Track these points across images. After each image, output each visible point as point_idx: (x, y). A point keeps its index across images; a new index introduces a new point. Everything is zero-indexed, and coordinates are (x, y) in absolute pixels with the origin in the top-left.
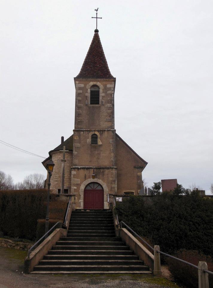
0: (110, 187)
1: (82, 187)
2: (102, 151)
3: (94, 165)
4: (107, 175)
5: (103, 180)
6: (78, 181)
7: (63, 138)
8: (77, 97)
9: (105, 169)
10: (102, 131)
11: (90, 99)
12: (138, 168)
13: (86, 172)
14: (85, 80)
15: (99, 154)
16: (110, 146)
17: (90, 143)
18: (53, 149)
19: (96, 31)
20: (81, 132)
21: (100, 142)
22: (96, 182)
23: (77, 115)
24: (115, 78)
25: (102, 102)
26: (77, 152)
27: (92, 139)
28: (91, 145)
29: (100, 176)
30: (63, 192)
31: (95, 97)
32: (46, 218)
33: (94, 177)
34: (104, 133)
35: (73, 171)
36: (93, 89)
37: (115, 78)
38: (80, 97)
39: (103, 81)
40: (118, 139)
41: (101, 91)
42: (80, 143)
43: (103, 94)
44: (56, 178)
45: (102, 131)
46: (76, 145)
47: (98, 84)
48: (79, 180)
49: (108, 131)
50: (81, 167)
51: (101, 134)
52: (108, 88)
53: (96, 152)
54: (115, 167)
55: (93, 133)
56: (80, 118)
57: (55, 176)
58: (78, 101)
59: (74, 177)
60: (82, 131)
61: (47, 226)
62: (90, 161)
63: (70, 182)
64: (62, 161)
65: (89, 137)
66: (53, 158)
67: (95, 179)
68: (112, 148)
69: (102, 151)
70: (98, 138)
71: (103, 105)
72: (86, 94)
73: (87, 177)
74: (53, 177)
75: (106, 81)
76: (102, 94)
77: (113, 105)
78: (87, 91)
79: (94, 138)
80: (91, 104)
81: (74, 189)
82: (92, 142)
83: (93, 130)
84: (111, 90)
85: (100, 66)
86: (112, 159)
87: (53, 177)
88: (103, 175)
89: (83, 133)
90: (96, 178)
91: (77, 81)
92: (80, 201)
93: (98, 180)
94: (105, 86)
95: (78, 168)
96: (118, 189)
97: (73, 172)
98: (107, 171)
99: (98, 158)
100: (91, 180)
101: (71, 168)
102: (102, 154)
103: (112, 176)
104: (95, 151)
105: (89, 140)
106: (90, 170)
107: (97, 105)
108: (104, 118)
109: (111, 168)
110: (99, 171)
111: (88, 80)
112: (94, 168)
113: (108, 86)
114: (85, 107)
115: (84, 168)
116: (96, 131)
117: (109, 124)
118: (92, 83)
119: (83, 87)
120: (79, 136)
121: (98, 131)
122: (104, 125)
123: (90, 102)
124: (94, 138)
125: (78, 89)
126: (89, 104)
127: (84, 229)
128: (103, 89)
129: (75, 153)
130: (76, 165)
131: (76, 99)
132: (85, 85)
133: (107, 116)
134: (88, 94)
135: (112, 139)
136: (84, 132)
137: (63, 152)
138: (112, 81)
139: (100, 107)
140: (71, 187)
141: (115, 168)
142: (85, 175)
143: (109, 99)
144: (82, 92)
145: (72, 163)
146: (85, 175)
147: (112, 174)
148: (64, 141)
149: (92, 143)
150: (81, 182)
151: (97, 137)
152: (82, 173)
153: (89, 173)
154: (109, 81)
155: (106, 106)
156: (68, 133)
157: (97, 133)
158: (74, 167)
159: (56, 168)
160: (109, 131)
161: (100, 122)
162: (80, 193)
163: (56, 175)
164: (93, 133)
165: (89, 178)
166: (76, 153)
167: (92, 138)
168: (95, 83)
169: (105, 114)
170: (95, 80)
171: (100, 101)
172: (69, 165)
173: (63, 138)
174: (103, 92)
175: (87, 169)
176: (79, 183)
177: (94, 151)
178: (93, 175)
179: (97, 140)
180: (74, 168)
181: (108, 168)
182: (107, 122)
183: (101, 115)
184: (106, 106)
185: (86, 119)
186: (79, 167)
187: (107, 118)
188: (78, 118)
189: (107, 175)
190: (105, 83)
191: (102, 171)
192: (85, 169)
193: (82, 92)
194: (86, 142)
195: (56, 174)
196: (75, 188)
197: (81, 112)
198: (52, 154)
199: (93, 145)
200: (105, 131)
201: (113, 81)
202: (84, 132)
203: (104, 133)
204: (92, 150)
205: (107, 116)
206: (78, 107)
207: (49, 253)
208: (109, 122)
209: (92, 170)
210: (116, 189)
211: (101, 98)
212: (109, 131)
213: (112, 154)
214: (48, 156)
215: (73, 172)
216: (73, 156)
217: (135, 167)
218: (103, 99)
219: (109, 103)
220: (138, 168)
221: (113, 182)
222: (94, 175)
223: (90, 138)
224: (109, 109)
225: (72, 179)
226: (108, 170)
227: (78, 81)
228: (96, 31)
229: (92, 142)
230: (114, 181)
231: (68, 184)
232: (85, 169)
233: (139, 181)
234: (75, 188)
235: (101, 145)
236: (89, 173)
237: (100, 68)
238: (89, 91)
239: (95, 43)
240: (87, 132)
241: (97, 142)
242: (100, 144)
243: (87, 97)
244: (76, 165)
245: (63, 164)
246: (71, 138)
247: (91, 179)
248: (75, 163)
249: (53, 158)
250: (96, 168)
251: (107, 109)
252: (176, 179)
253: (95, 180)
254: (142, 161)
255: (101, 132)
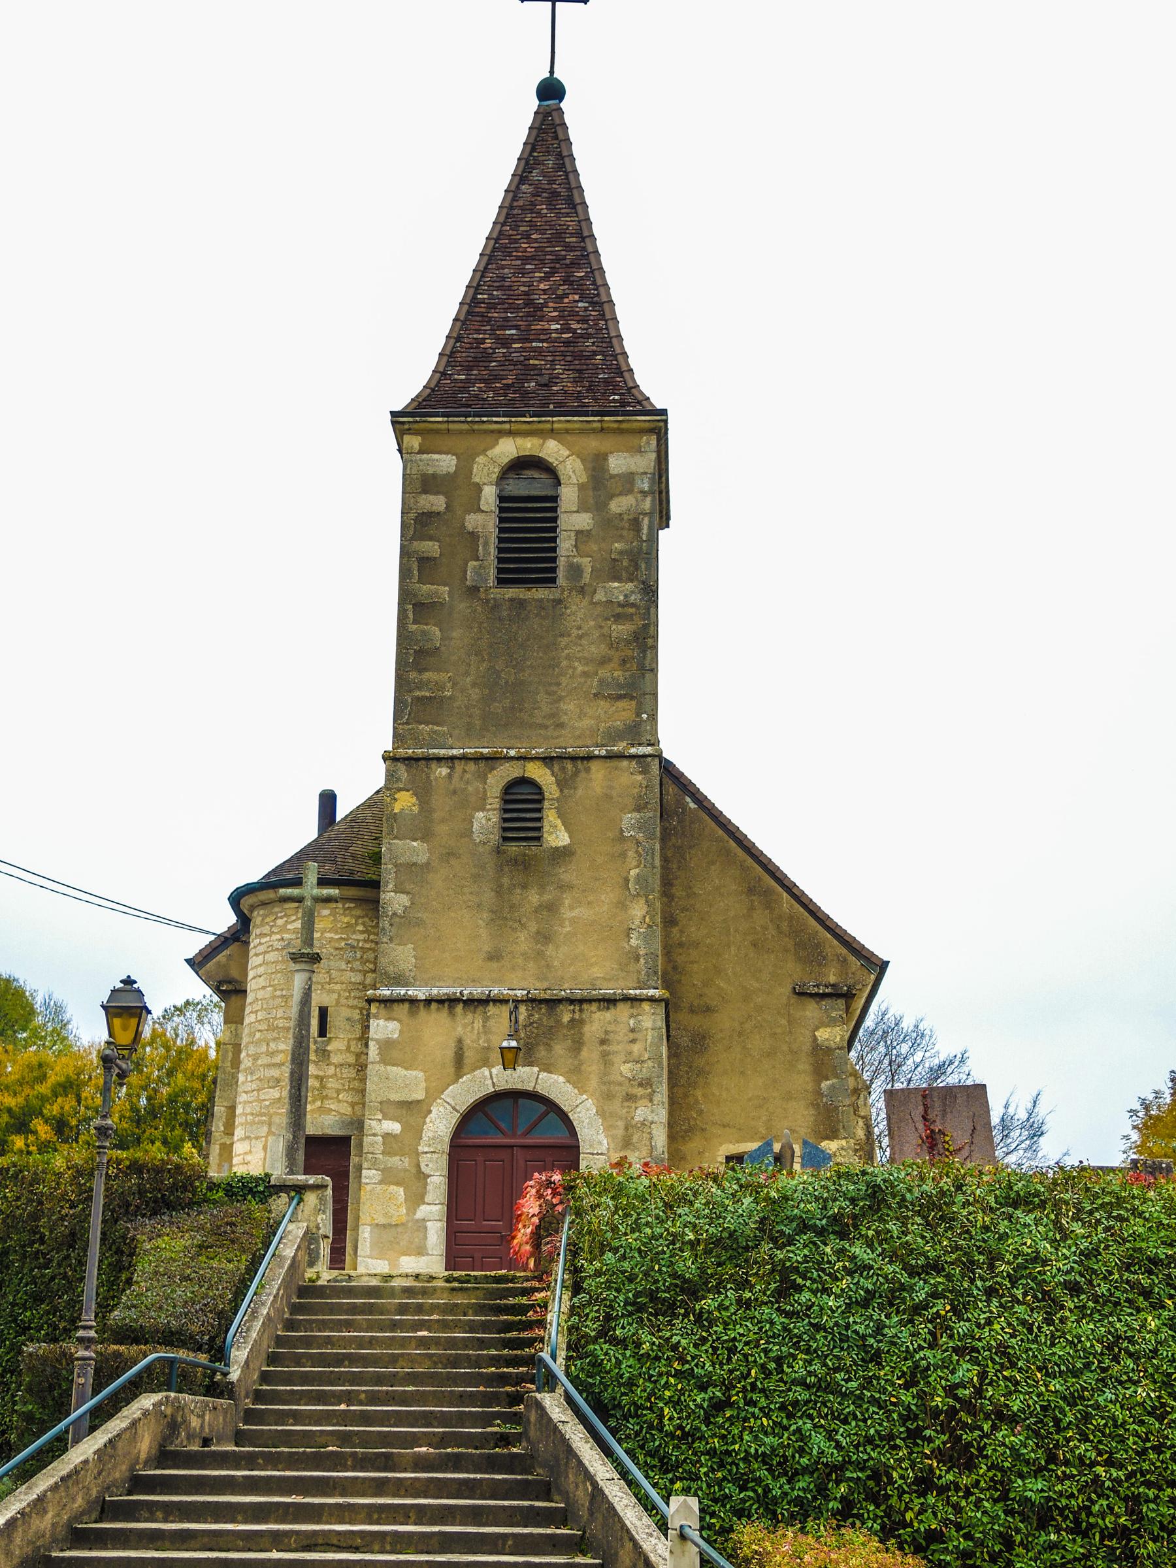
0: (621, 1124)
1: (440, 1124)
2: (571, 887)
3: (517, 983)
4: (603, 1042)
5: (575, 1075)
6: (408, 1082)
7: (328, 801)
8: (412, 539)
9: (585, 1006)
10: (569, 763)
11: (493, 551)
12: (824, 996)
13: (467, 1026)
14: (465, 427)
15: (551, 908)
16: (623, 855)
17: (495, 837)
18: (255, 876)
19: (551, 91)
20: (434, 765)
21: (557, 836)
22: (529, 1087)
23: (413, 657)
24: (664, 412)
25: (575, 571)
26: (408, 893)
27: (506, 811)
28: (498, 851)
29: (559, 1049)
30: (300, 1156)
31: (528, 538)
32: (80, 1333)
33: (510, 1059)
34: (588, 770)
35: (376, 1017)
36: (516, 488)
37: (664, 412)
38: (431, 538)
39: (582, 432)
40: (692, 805)
41: (568, 495)
42: (426, 835)
43: (584, 521)
44: (274, 1065)
45: (574, 758)
46: (405, 849)
47: (552, 450)
48: (421, 1075)
49: (610, 757)
50: (435, 991)
51: (561, 784)
52: (612, 477)
53: (534, 898)
54: (651, 992)
55: (511, 771)
56: (427, 675)
57: (264, 1049)
58: (415, 567)
59: (385, 1061)
60: (439, 759)
61: (83, 1379)
62: (494, 956)
63: (363, 1092)
64: (295, 957)
65: (484, 799)
66: (255, 931)
67: (522, 1071)
68: (633, 872)
69: (571, 887)
70: (546, 804)
71: (582, 591)
72: (473, 521)
73: (470, 1056)
74: (256, 1058)
75: (602, 429)
76: (573, 518)
77: (650, 592)
78: (479, 499)
79: (522, 806)
80: (501, 582)
81: (386, 1136)
82: (505, 829)
83: (512, 753)
84: (630, 491)
85: (566, 329)
86: (633, 942)
87: (256, 1058)
88: (578, 1045)
89: (450, 776)
90: (531, 1064)
91: (409, 431)
92: (423, 1211)
93: (543, 1075)
94: (597, 466)
95: (413, 1001)
96: (672, 1137)
97: (382, 1022)
98: (597, 1021)
99: (544, 937)
100: (492, 1078)
101: (370, 1001)
102: (571, 908)
103: (636, 1048)
104: (524, 887)
105: (485, 821)
106: (492, 1009)
107: (541, 593)
108: (584, 674)
109: (626, 999)
110: (548, 1018)
111: (485, 427)
112: (517, 1002)
113: (618, 463)
114: (462, 606)
115: (450, 1002)
116: (532, 759)
117: (623, 712)
118: (507, 449)
119: (448, 474)
120: (423, 793)
121: (547, 760)
122: (584, 720)
123: (493, 573)
124: (522, 806)
125: (416, 484)
126: (491, 581)
127: (461, 1395)
128: (582, 487)
129: (394, 900)
130: (399, 980)
131: (405, 552)
132: (466, 461)
133: (604, 661)
134: (484, 521)
135: (638, 809)
136: (452, 768)
137: (300, 900)
138: (642, 432)
139: (560, 601)
140: (367, 1122)
141: (651, 1000)
142: (460, 1041)
143: (621, 553)
144: (442, 508)
145: (375, 970)
146: (460, 1041)
147: (631, 1036)
148: (338, 818)
149: (505, 839)
150: (434, 1094)
151: (540, 801)
152: (438, 1032)
153: (486, 1030)
154: (621, 431)
155: (600, 596)
156: (663, 534)
157: (535, 771)
158: (385, 992)
159: (274, 997)
160: (621, 756)
161: (561, 699)
162: (424, 1160)
163: (273, 1046)
164: (516, 775)
165: (486, 1062)
166: (404, 899)
167: (506, 802)
168: (528, 446)
169: (593, 649)
170: (525, 427)
171: (561, 562)
172: (357, 978)
173: (328, 801)
174: (583, 508)
175: (472, 1003)
176: (419, 1095)
177: (518, 891)
178: (505, 1044)
179: (539, 819)
180: (387, 1002)
181: (609, 1002)
182: (602, 703)
183: (568, 657)
184: (600, 596)
185: (468, 680)
186: (420, 993)
187: (604, 673)
188: (413, 675)
189: (603, 1042)
190: (594, 444)
191: (566, 1018)
192: (459, 1008)
193: (442, 508)
194: (469, 833)
195: (275, 1035)
196: (395, 1127)
197: (438, 633)
198: (252, 908)
199: (513, 848)
200: (589, 758)
201: (651, 431)
202: (452, 768)
203: (583, 775)
204: (505, 881)
205: (604, 661)
206: (414, 607)
207: (106, 1510)
208: (620, 697)
209: (505, 1010)
210: (660, 1138)
211: (565, 545)
212: (621, 756)
213: (638, 910)
214: (226, 919)
215: (383, 1028)
216: (385, 923)
217: (801, 994)
218: (582, 547)
219: (617, 578)
220: (824, 996)
221: (640, 1091)
222: (514, 1044)
223: (494, 802)
224: (618, 618)
225: (374, 1070)
226: (608, 1015)
227: (417, 433)
228: (551, 91)
229: (505, 829)
230: (646, 1083)
231: (353, 1105)
232: (459, 1008)
233: (825, 1084)
234: (395, 1127)
235: (562, 855)
236: (486, 1030)
237: (567, 343)
238: (489, 495)
239: (535, 175)
240: (471, 766)
241: (539, 829)
242: (561, 844)
243: (474, 536)
244: (399, 980)
245: (299, 980)
246: (375, 805)
247: (494, 1071)
248: (391, 969)
249: (258, 931)
250: (531, 1001)
251: (607, 619)
252: (983, 1087)
253: (524, 1077)
254: (844, 951)
255: (563, 769)
